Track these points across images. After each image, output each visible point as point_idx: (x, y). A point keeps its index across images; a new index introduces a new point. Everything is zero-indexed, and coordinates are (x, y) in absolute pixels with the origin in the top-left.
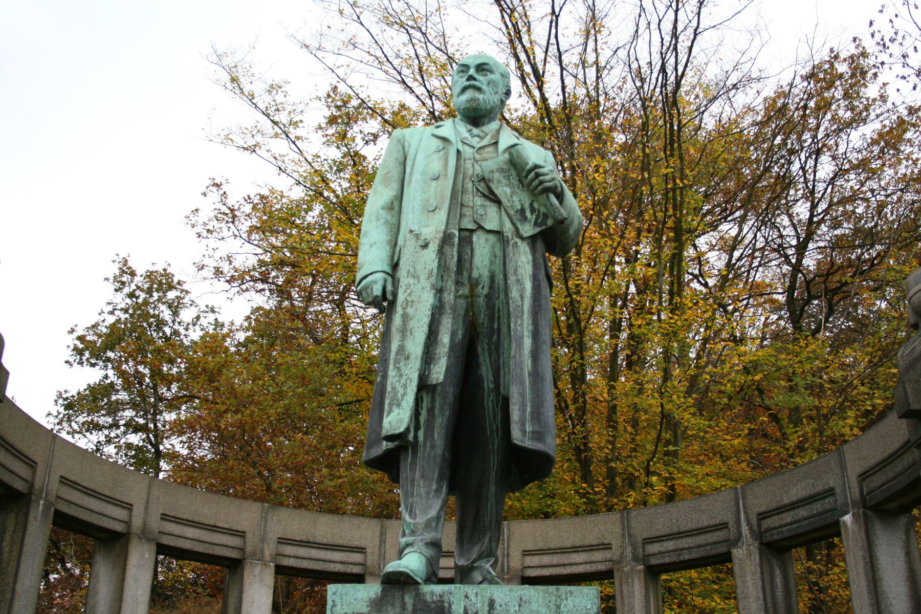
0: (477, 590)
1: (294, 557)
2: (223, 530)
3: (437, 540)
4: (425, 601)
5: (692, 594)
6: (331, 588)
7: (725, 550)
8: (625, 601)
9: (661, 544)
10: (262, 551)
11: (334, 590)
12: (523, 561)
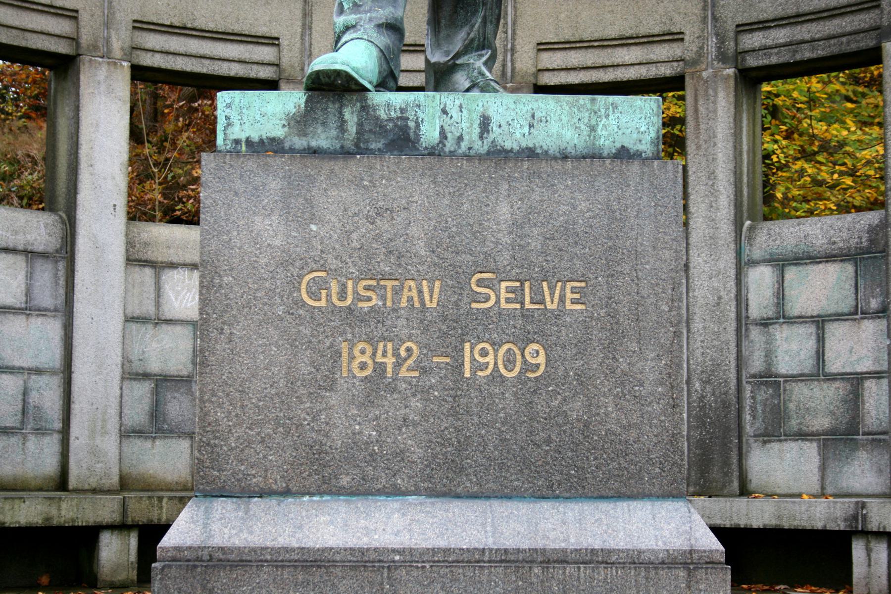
0: (462, 101)
1: (162, 52)
2: (40, 8)
3: (396, 19)
4: (378, 118)
5: (810, 117)
6: (223, 97)
7: (872, 43)
8: (701, 126)
9: (767, 33)
10: (108, 41)
11: (228, 101)
12: (537, 59)
